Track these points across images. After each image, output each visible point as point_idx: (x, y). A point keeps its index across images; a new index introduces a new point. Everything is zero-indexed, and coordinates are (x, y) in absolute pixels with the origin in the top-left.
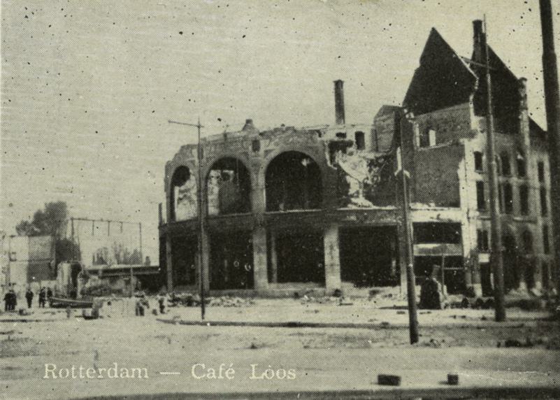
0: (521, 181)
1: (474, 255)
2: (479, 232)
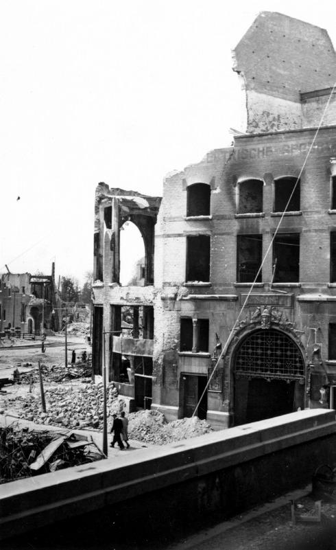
1: (170, 362)
2: (185, 322)
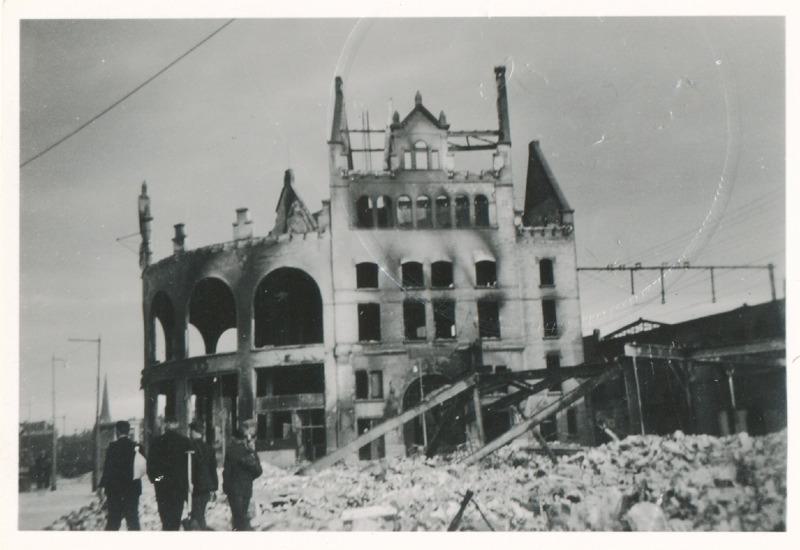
0: (439, 294)
